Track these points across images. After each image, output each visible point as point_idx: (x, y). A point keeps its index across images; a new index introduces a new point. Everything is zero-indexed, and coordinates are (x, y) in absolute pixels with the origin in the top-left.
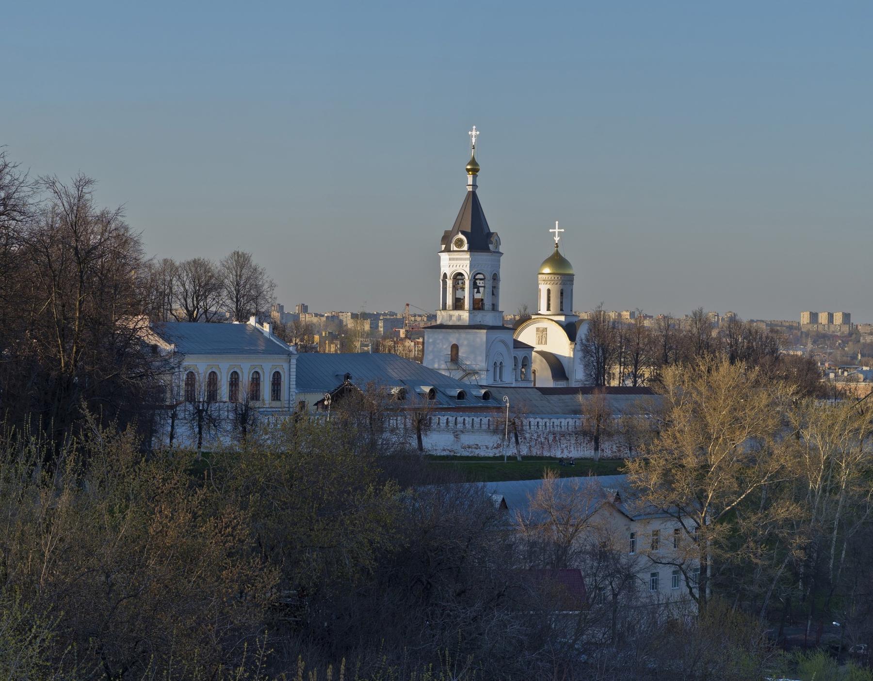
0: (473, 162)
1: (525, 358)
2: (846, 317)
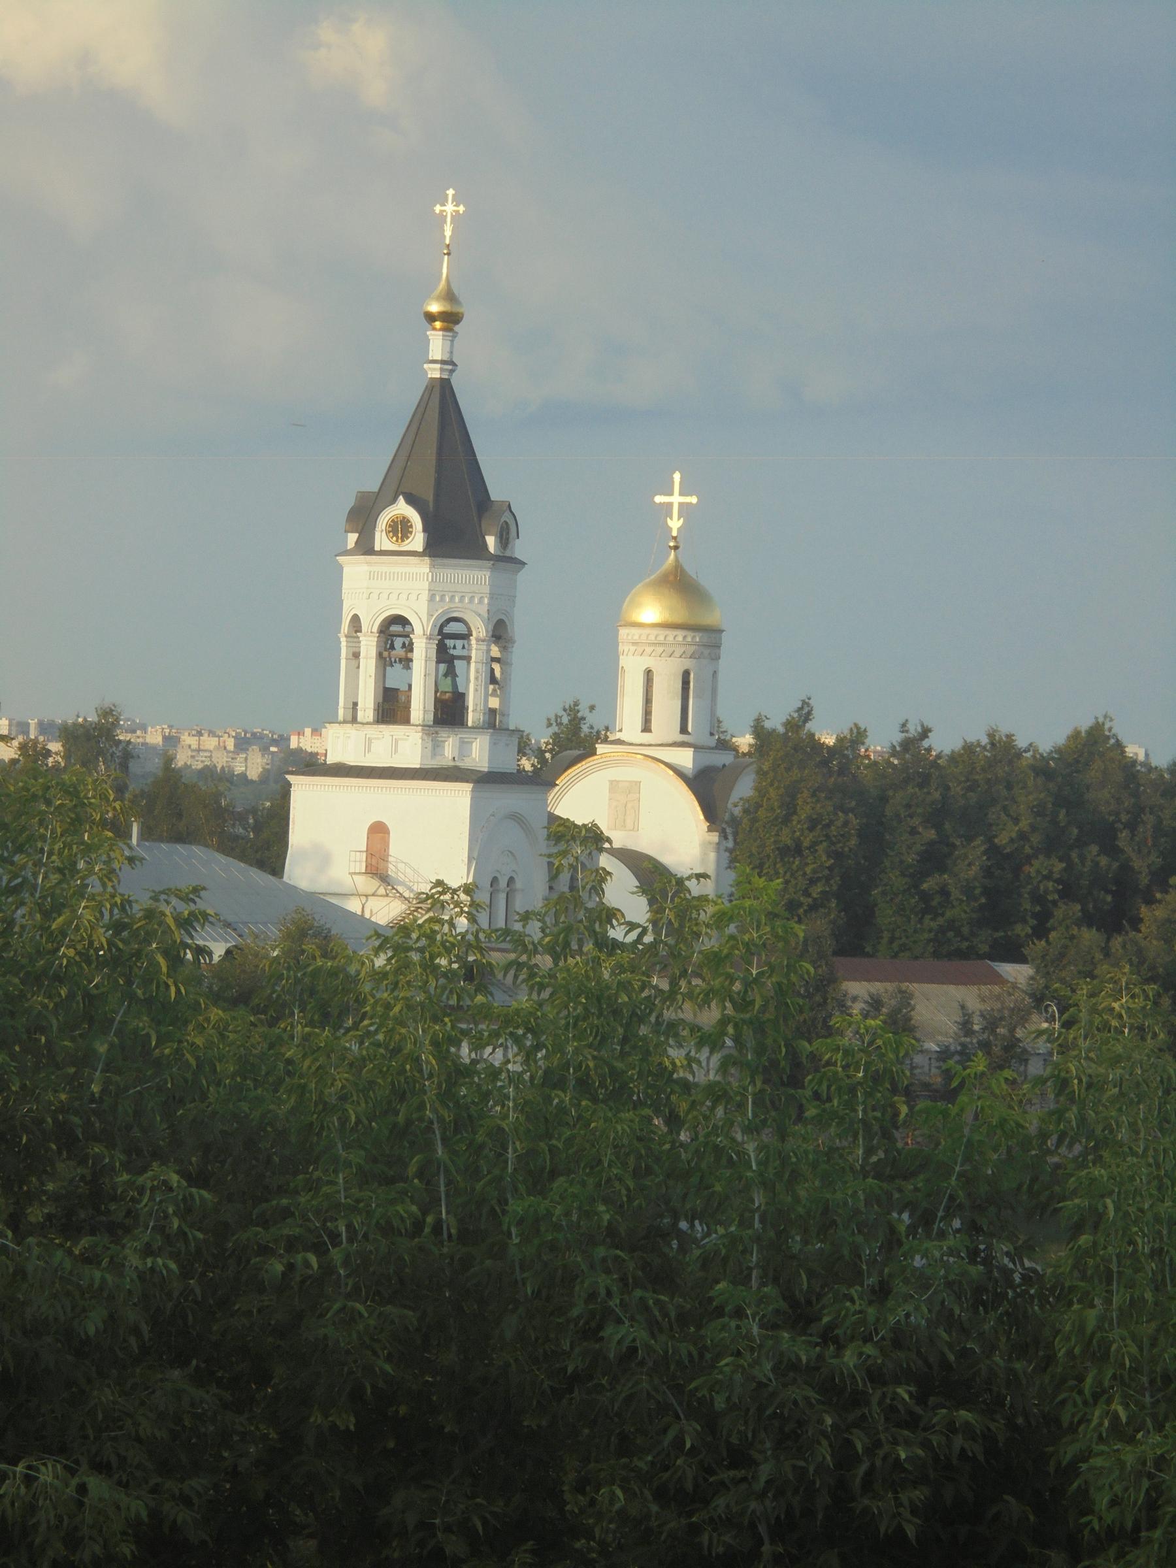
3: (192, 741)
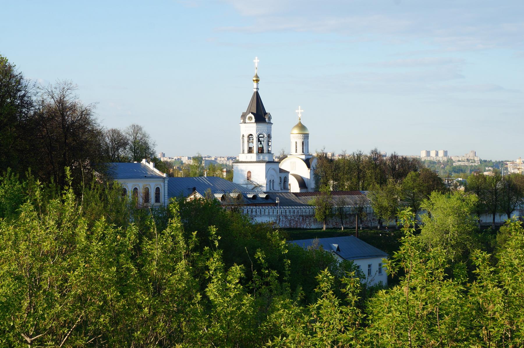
0: (257, 76)
1: (285, 177)
2: (446, 153)
3: (220, 159)
